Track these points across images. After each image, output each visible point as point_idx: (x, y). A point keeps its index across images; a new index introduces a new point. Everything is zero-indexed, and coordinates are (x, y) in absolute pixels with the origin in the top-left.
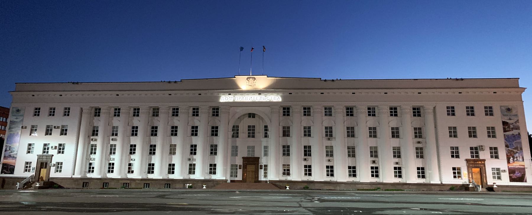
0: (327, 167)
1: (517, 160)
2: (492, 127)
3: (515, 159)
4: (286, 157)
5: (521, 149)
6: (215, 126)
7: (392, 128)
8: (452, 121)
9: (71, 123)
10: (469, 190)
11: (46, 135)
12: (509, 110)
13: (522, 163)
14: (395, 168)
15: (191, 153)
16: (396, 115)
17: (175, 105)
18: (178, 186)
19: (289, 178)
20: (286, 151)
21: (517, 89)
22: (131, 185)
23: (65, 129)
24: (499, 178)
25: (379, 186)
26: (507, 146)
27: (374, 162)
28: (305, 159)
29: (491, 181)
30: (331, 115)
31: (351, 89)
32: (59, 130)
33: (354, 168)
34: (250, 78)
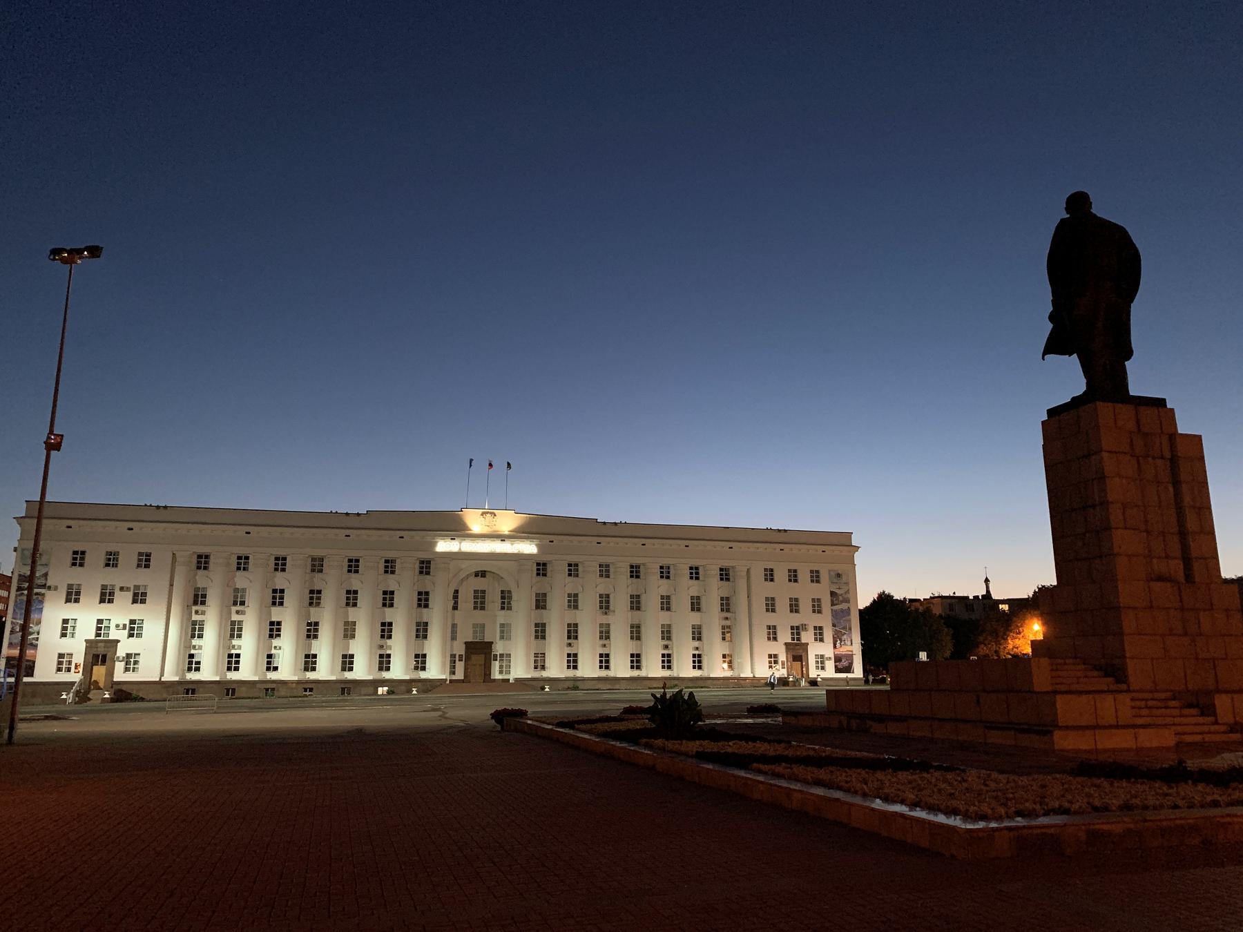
0: (601, 655)
1: (845, 644)
2: (818, 599)
3: (843, 643)
4: (540, 641)
5: (850, 629)
6: (423, 590)
7: (692, 598)
8: (769, 589)
9: (150, 579)
10: (788, 685)
11: (66, 602)
12: (839, 575)
13: (850, 648)
14: (694, 656)
15: (382, 637)
16: (697, 578)
17: (354, 554)
18: (364, 691)
19: (545, 674)
20: (540, 632)
21: (850, 548)
22: (278, 690)
23: (140, 592)
24: (823, 668)
25: (676, 682)
26: (834, 625)
27: (666, 647)
28: (570, 645)
29: (813, 673)
30: (608, 576)
31: (342, 528)
32: (130, 595)
33: (638, 655)
34: (487, 513)
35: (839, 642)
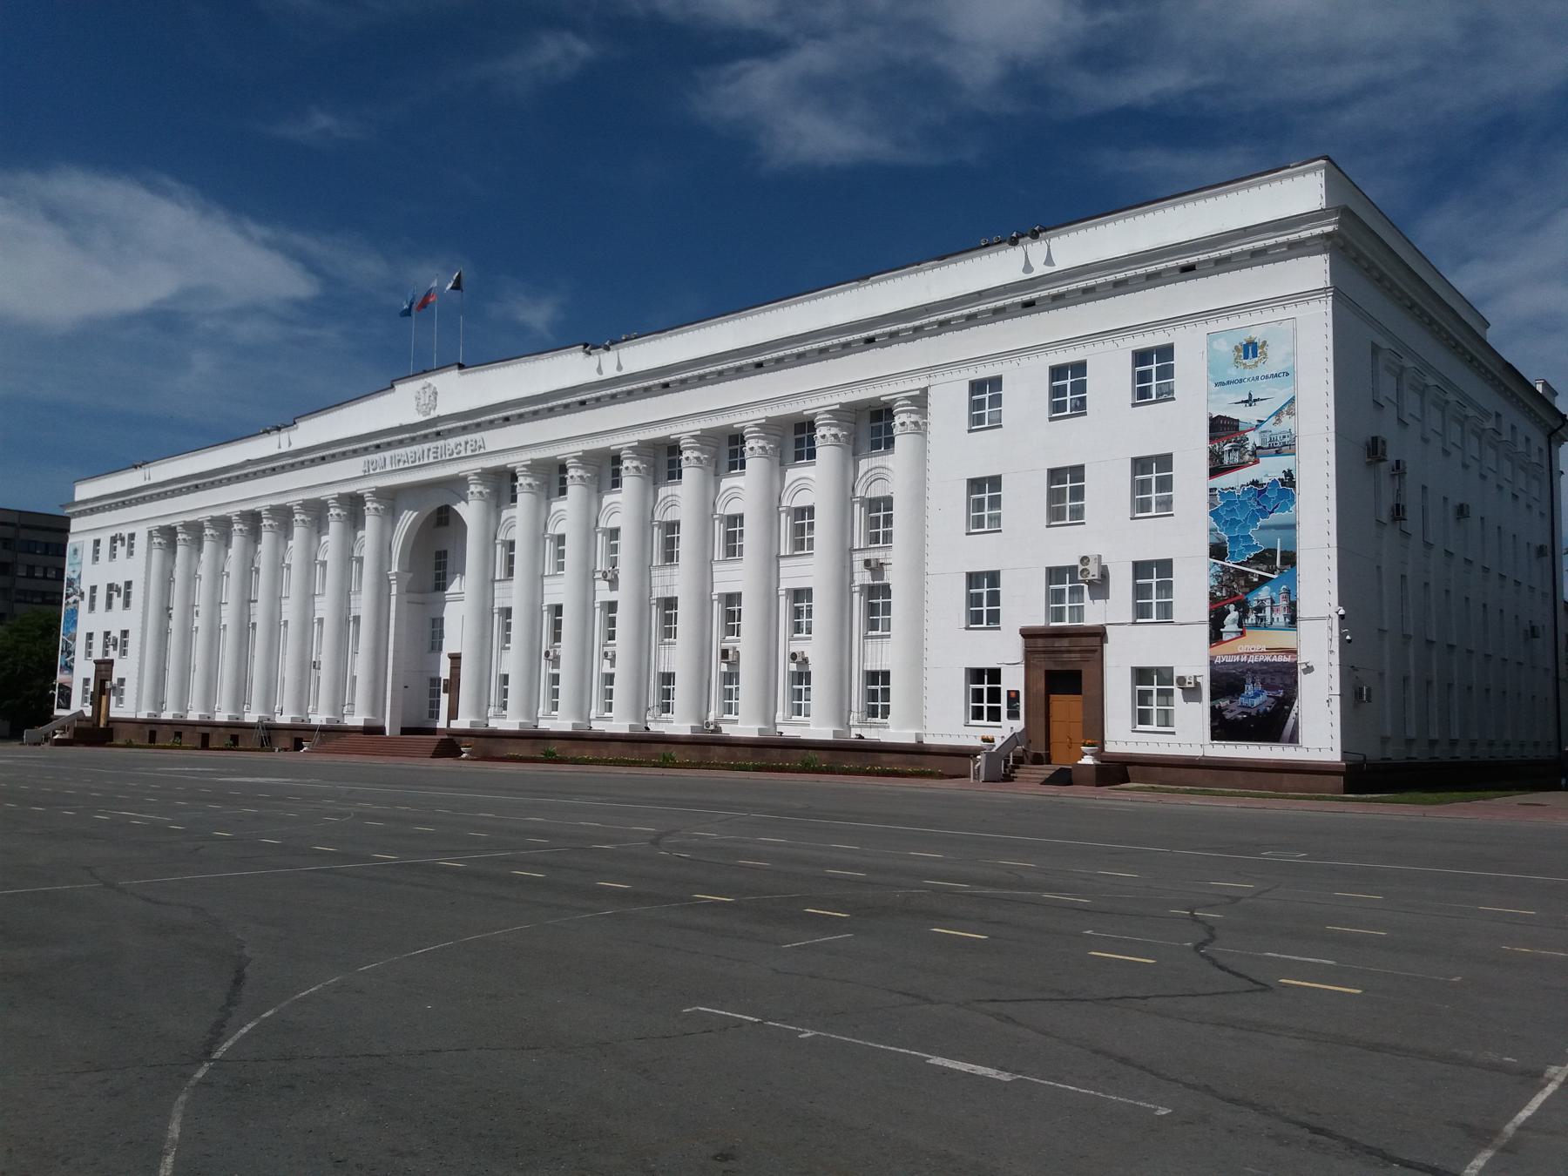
1: (1260, 624)
3: (1252, 618)
13: (1284, 639)
35: (1234, 615)
